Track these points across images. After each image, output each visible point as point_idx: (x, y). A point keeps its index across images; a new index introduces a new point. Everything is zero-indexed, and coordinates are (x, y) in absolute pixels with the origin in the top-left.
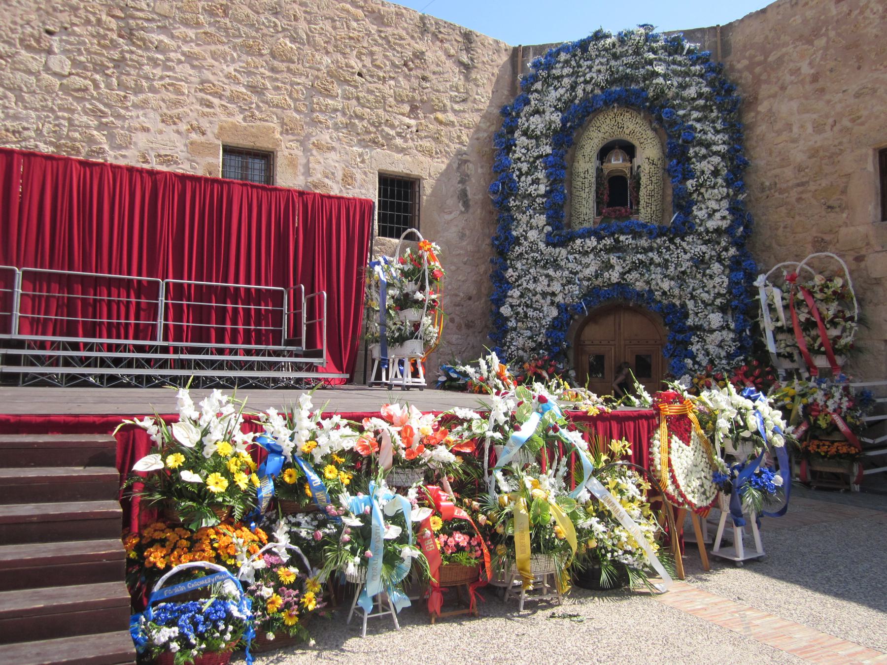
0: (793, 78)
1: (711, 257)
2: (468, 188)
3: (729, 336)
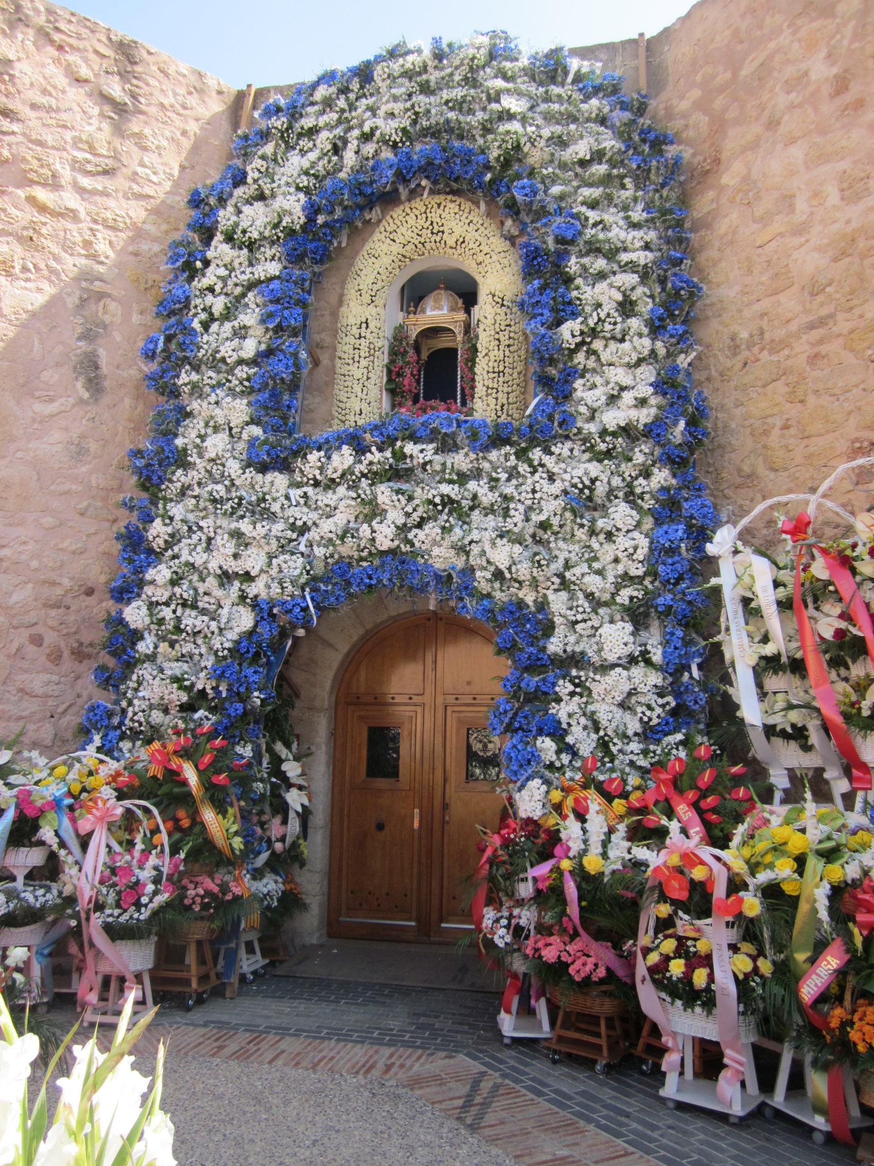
0: (793, 95)
1: (611, 493)
2: (102, 352)
3: (647, 680)
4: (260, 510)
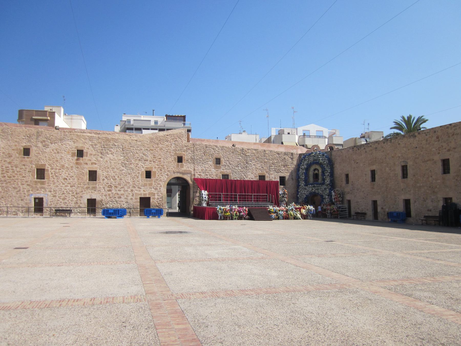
4: (305, 189)
